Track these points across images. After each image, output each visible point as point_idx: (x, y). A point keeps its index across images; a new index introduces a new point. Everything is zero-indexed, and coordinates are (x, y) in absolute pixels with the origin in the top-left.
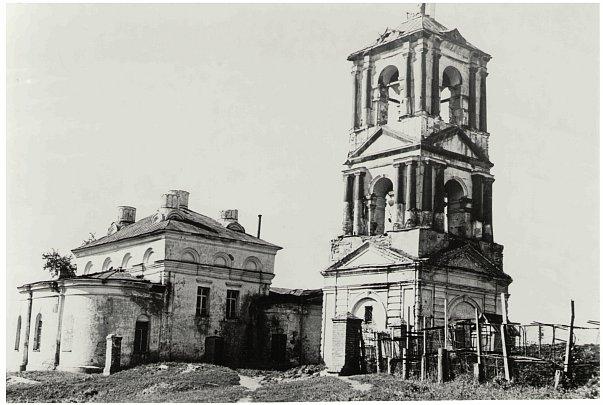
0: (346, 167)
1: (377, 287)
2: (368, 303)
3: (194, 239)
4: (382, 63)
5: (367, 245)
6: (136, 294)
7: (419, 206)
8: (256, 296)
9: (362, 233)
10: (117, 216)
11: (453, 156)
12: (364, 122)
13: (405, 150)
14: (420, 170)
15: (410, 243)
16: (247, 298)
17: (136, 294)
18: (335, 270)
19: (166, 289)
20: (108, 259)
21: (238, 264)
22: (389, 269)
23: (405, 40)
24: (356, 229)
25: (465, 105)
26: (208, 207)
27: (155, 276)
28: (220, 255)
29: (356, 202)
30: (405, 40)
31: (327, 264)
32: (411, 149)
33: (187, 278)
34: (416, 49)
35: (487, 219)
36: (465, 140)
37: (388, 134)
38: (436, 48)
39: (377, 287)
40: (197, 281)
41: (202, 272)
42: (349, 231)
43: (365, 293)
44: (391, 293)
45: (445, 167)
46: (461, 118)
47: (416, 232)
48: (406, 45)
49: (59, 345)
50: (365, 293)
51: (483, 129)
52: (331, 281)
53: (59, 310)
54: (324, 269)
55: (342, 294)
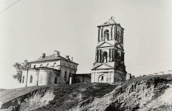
0: (96, 49)
1: (105, 72)
2: (102, 76)
3: (65, 61)
4: (105, 29)
5: (103, 64)
6: (55, 72)
7: (114, 57)
8: (74, 74)
9: (100, 62)
10: (42, 55)
11: (119, 48)
12: (101, 40)
13: (111, 46)
14: (114, 51)
15: (112, 64)
16: (73, 74)
17: (55, 72)
18: (95, 69)
19: (59, 71)
20: (42, 64)
21: (71, 67)
22: (108, 69)
23: (111, 25)
24: (99, 61)
25: (120, 38)
26: (63, 55)
27: (58, 68)
28: (69, 65)
29: (99, 56)
30: (111, 25)
31: (92, 68)
32: (112, 46)
33: (63, 69)
34: (113, 27)
35: (123, 61)
36: (120, 45)
37: (106, 43)
38: (117, 27)
39: (105, 72)
40: (65, 70)
41: (66, 68)
42: (97, 61)
43: (102, 74)
44: (108, 74)
45: (118, 50)
46: (119, 41)
47: (114, 62)
48: (111, 26)
49: (38, 82)
50: (102, 74)
51: (123, 43)
52: (94, 71)
53: (38, 74)
54: (92, 69)
55: (96, 74)
